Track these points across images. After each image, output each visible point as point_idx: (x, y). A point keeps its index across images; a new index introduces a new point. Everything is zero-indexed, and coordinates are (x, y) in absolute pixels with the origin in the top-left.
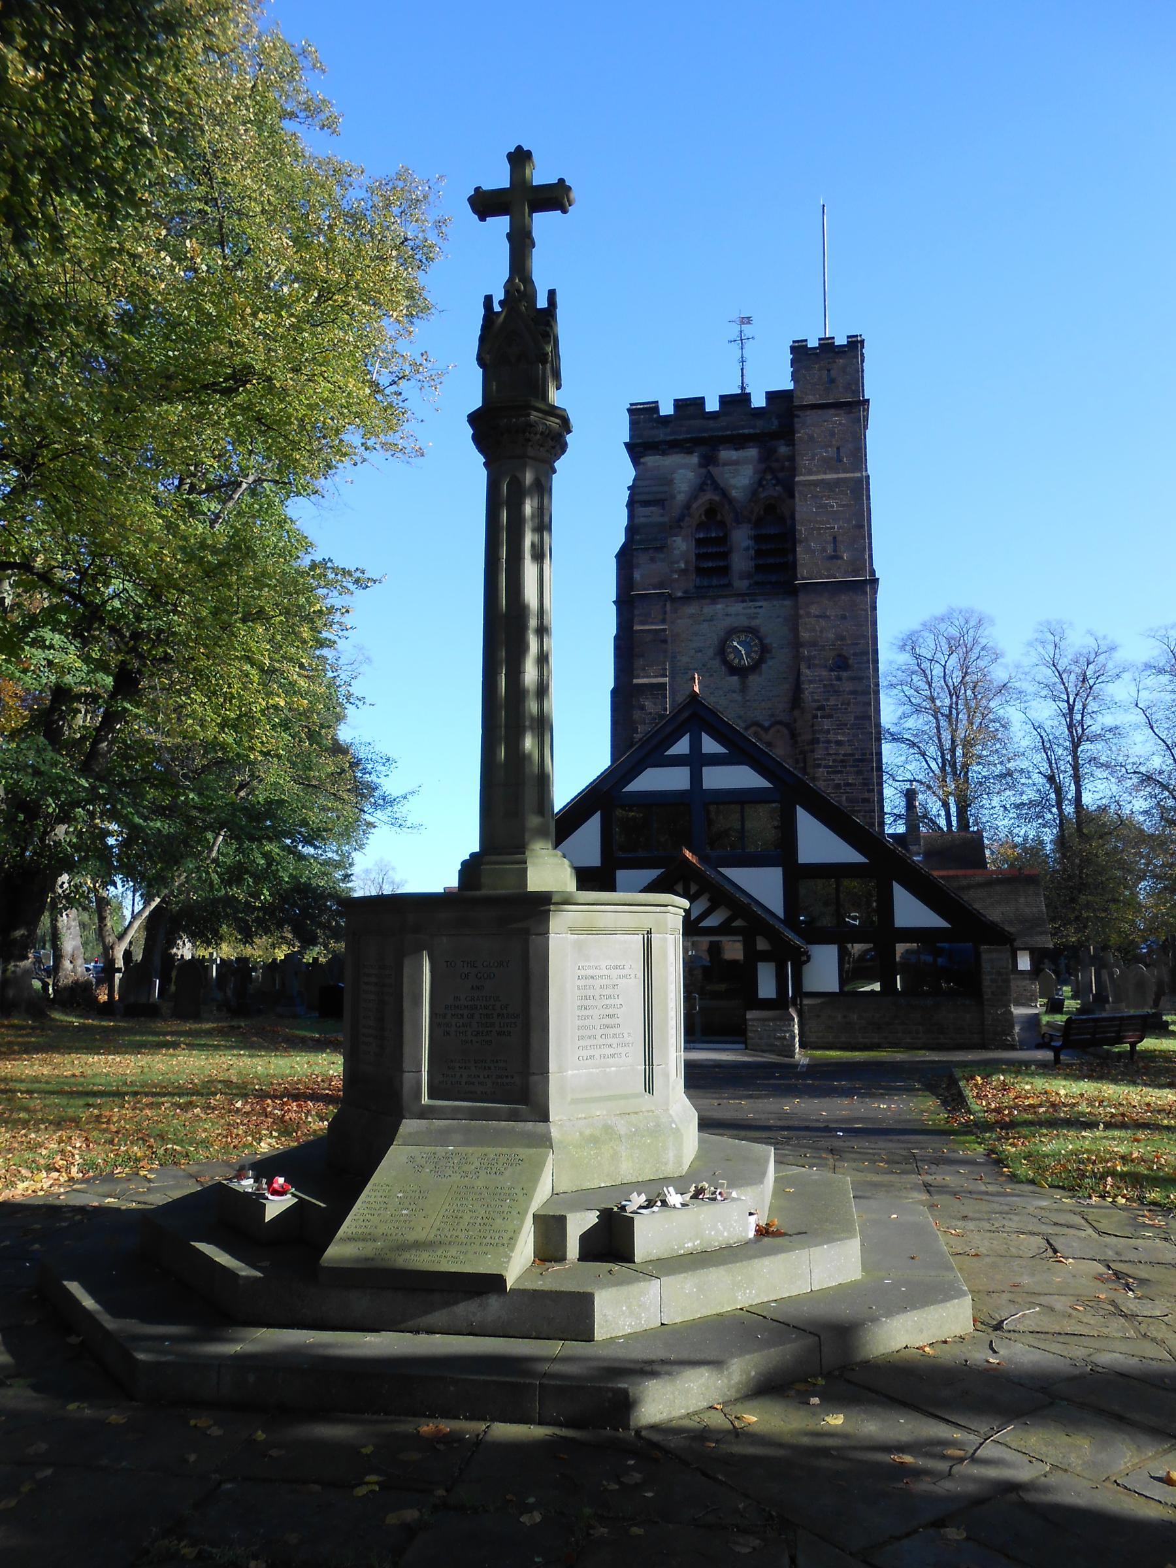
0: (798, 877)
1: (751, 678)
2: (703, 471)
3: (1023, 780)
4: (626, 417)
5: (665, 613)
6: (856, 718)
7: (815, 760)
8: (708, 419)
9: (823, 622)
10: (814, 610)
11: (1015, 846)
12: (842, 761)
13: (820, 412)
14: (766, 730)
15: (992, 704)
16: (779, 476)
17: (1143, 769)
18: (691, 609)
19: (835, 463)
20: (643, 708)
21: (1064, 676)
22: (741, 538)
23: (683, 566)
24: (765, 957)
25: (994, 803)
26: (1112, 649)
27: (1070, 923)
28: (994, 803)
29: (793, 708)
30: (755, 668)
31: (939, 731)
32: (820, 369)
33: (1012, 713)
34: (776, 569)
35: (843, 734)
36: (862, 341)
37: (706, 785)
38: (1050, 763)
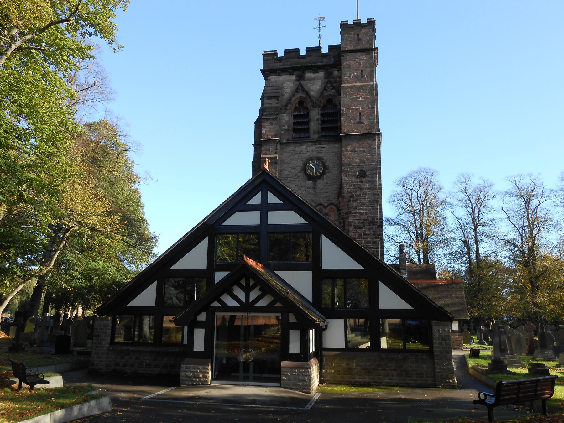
0: (322, 277)
1: (318, 182)
2: (298, 83)
3: (453, 242)
5: (277, 149)
7: (349, 222)
8: (300, 58)
9: (354, 154)
10: (350, 148)
11: (449, 272)
12: (362, 223)
13: (354, 54)
14: (325, 207)
15: (438, 209)
16: (334, 85)
17: (506, 238)
18: (290, 148)
19: (361, 78)
21: (470, 197)
22: (315, 114)
24: (294, 327)
25: (440, 253)
26: (491, 185)
28: (440, 253)
29: (338, 197)
30: (320, 177)
31: (415, 221)
32: (354, 34)
33: (448, 214)
34: (332, 129)
35: (363, 209)
36: (374, 21)
38: (464, 235)
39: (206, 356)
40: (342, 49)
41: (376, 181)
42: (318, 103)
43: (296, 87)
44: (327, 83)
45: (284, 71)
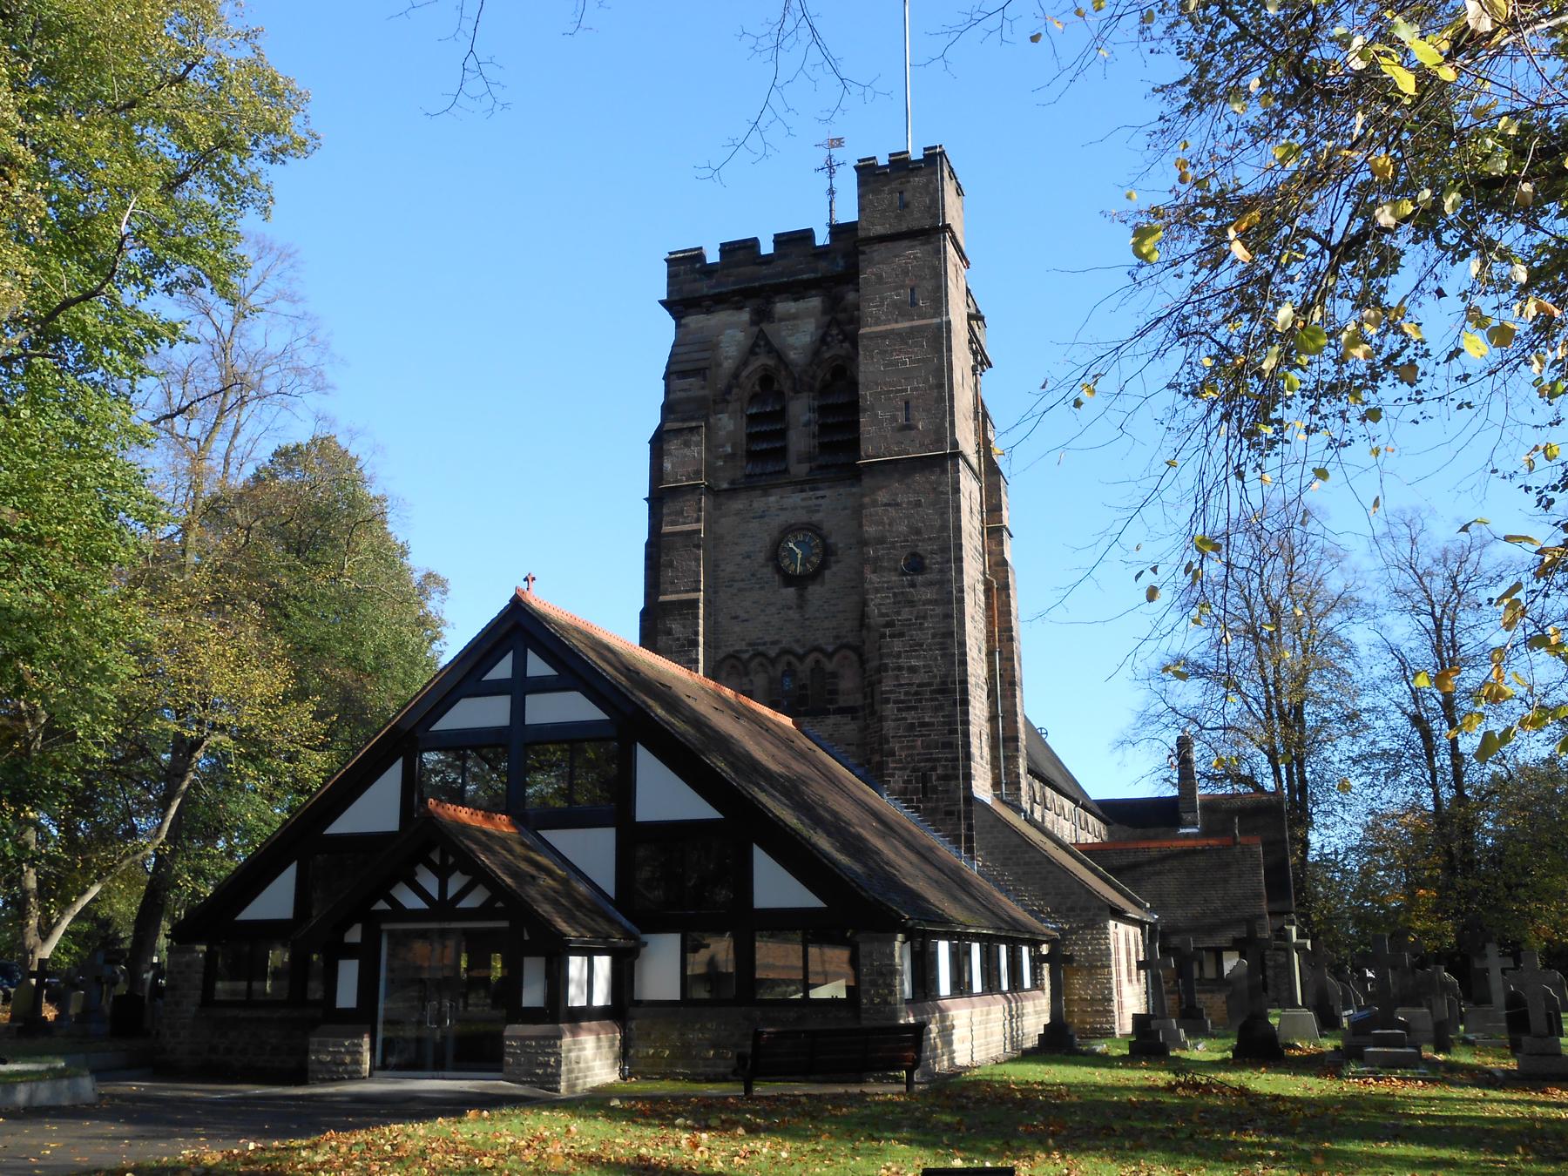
0: (637, 841)
1: (811, 589)
2: (755, 329)
4: (663, 270)
8: (760, 264)
10: (882, 496)
12: (916, 693)
13: (890, 245)
14: (830, 656)
16: (842, 325)
18: (738, 504)
19: (909, 308)
20: (669, 632)
21: (1426, 580)
22: (800, 410)
23: (729, 449)
30: (815, 575)
32: (890, 193)
33: (1360, 634)
34: (839, 452)
35: (918, 657)
36: (942, 153)
39: (363, 1017)
40: (861, 234)
41: (950, 581)
42: (806, 384)
43: (750, 342)
44: (829, 325)
45: (718, 301)
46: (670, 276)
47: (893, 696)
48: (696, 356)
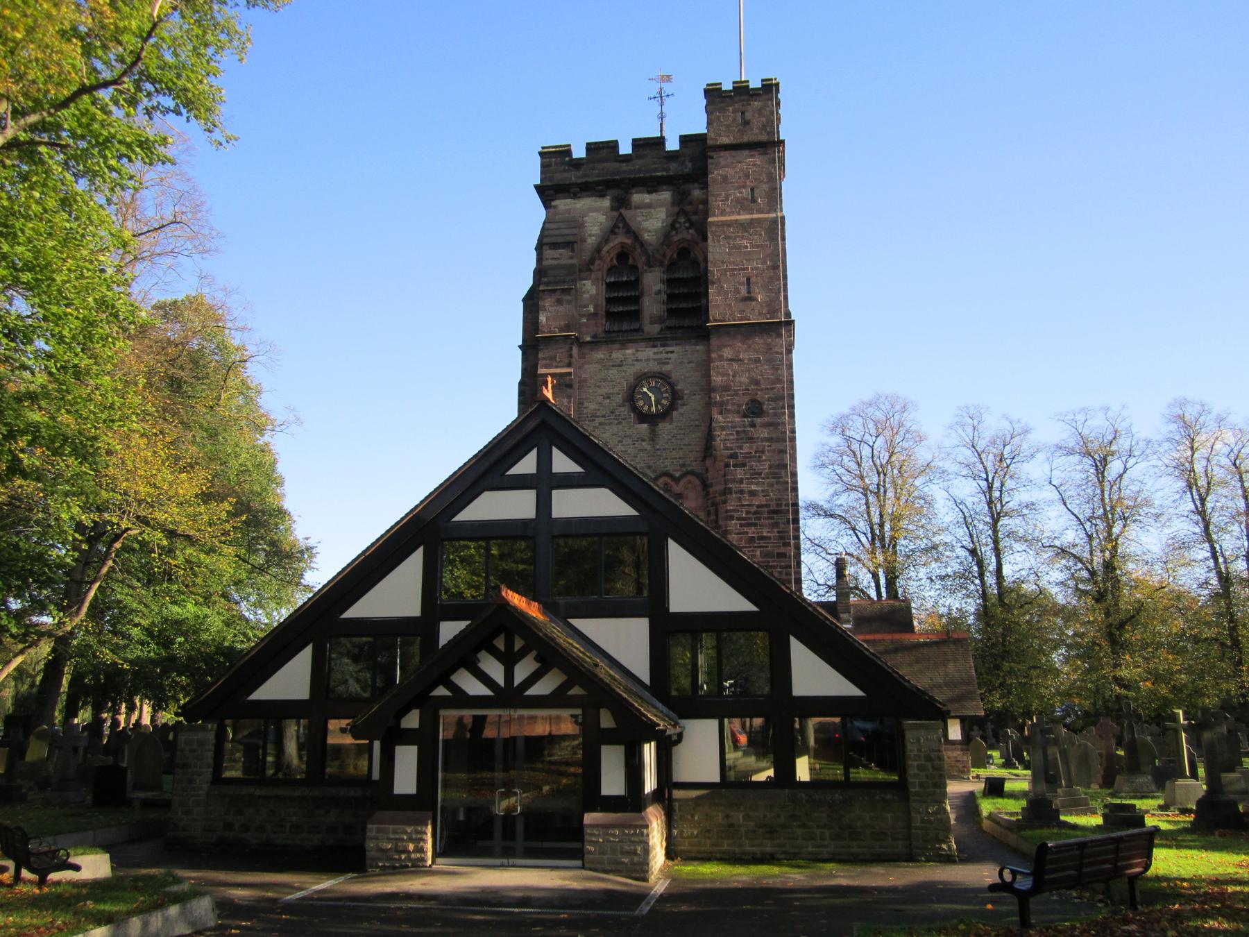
0: (670, 631)
1: (660, 425)
2: (615, 214)
3: (948, 553)
4: (538, 160)
5: (571, 356)
6: (770, 467)
7: (727, 511)
10: (727, 353)
11: (942, 616)
12: (755, 513)
13: (734, 153)
14: (677, 480)
15: (917, 483)
16: (692, 219)
17: (1057, 543)
18: (600, 355)
21: (983, 456)
22: (653, 281)
24: (611, 738)
25: (921, 575)
26: (1026, 431)
27: (995, 689)
28: (921, 575)
29: (704, 458)
30: (665, 415)
32: (735, 111)
33: (936, 492)
34: (688, 314)
35: (757, 484)
36: (777, 85)
37: (556, 513)
39: (421, 803)
40: (710, 142)
41: (784, 424)
43: (611, 224)
44: (678, 214)
45: (586, 189)
46: (543, 166)
47: (736, 515)
48: (566, 232)
